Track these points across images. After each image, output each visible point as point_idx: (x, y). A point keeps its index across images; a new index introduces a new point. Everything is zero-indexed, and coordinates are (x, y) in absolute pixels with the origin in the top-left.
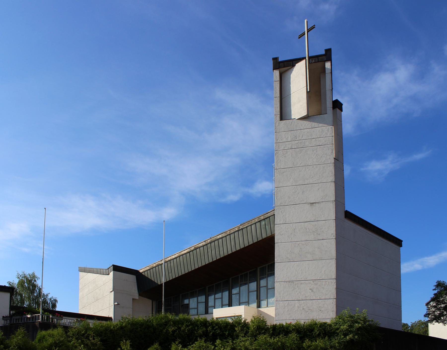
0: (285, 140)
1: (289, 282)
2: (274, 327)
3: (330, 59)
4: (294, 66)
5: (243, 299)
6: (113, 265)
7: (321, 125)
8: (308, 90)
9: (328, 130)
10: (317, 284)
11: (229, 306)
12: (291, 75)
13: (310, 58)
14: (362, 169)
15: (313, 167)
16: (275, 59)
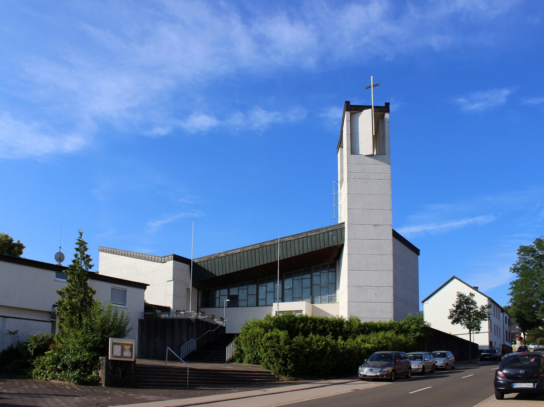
1: (359, 287)
2: (366, 325)
3: (388, 111)
4: (362, 111)
5: (297, 294)
6: (174, 255)
7: (382, 163)
12: (359, 118)
13: (375, 107)
14: (321, 115)
16: (347, 103)
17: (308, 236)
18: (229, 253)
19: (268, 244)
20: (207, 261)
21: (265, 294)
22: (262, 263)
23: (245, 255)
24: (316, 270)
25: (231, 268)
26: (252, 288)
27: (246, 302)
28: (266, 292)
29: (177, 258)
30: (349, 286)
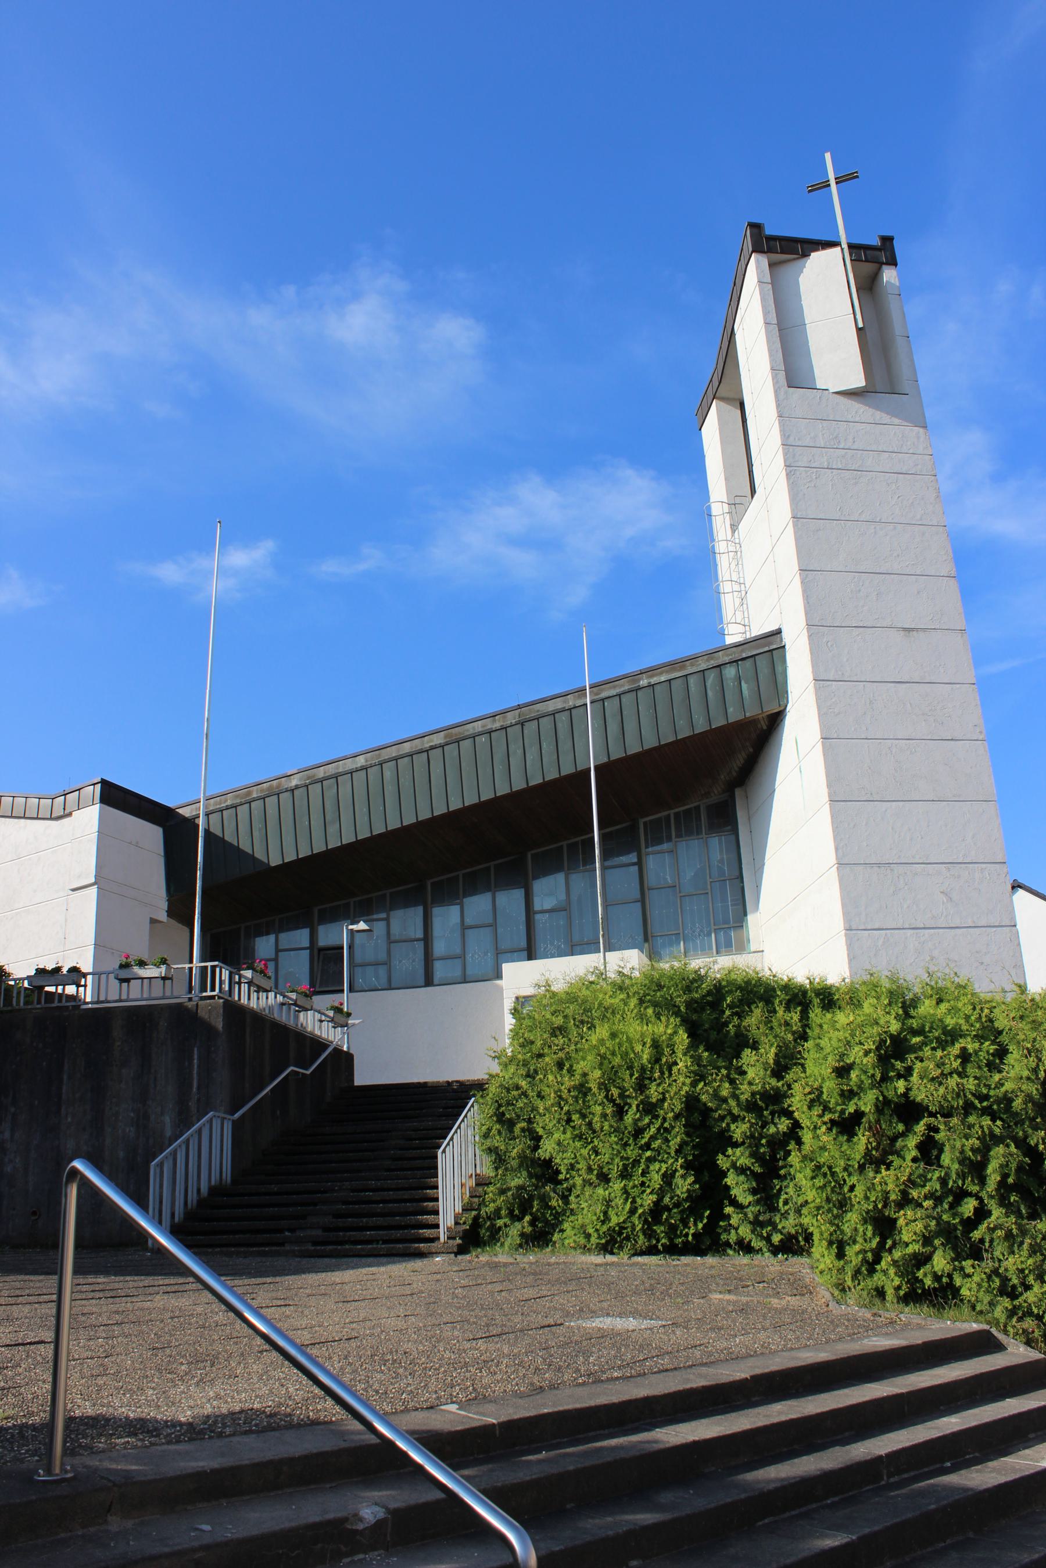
0: (807, 441)
1: (879, 865)
4: (805, 255)
6: (104, 782)
7: (896, 421)
8: (861, 325)
9: (918, 438)
10: (959, 877)
11: (530, 957)
12: (801, 279)
15: (895, 528)
16: (756, 228)
17: (638, 689)
18: (321, 773)
19: (478, 727)
20: (235, 807)
21: (457, 935)
22: (455, 805)
23: (387, 774)
24: (658, 835)
25: (332, 829)
26: (407, 921)
27: (382, 971)
28: (464, 927)
29: (113, 796)
30: (841, 864)
